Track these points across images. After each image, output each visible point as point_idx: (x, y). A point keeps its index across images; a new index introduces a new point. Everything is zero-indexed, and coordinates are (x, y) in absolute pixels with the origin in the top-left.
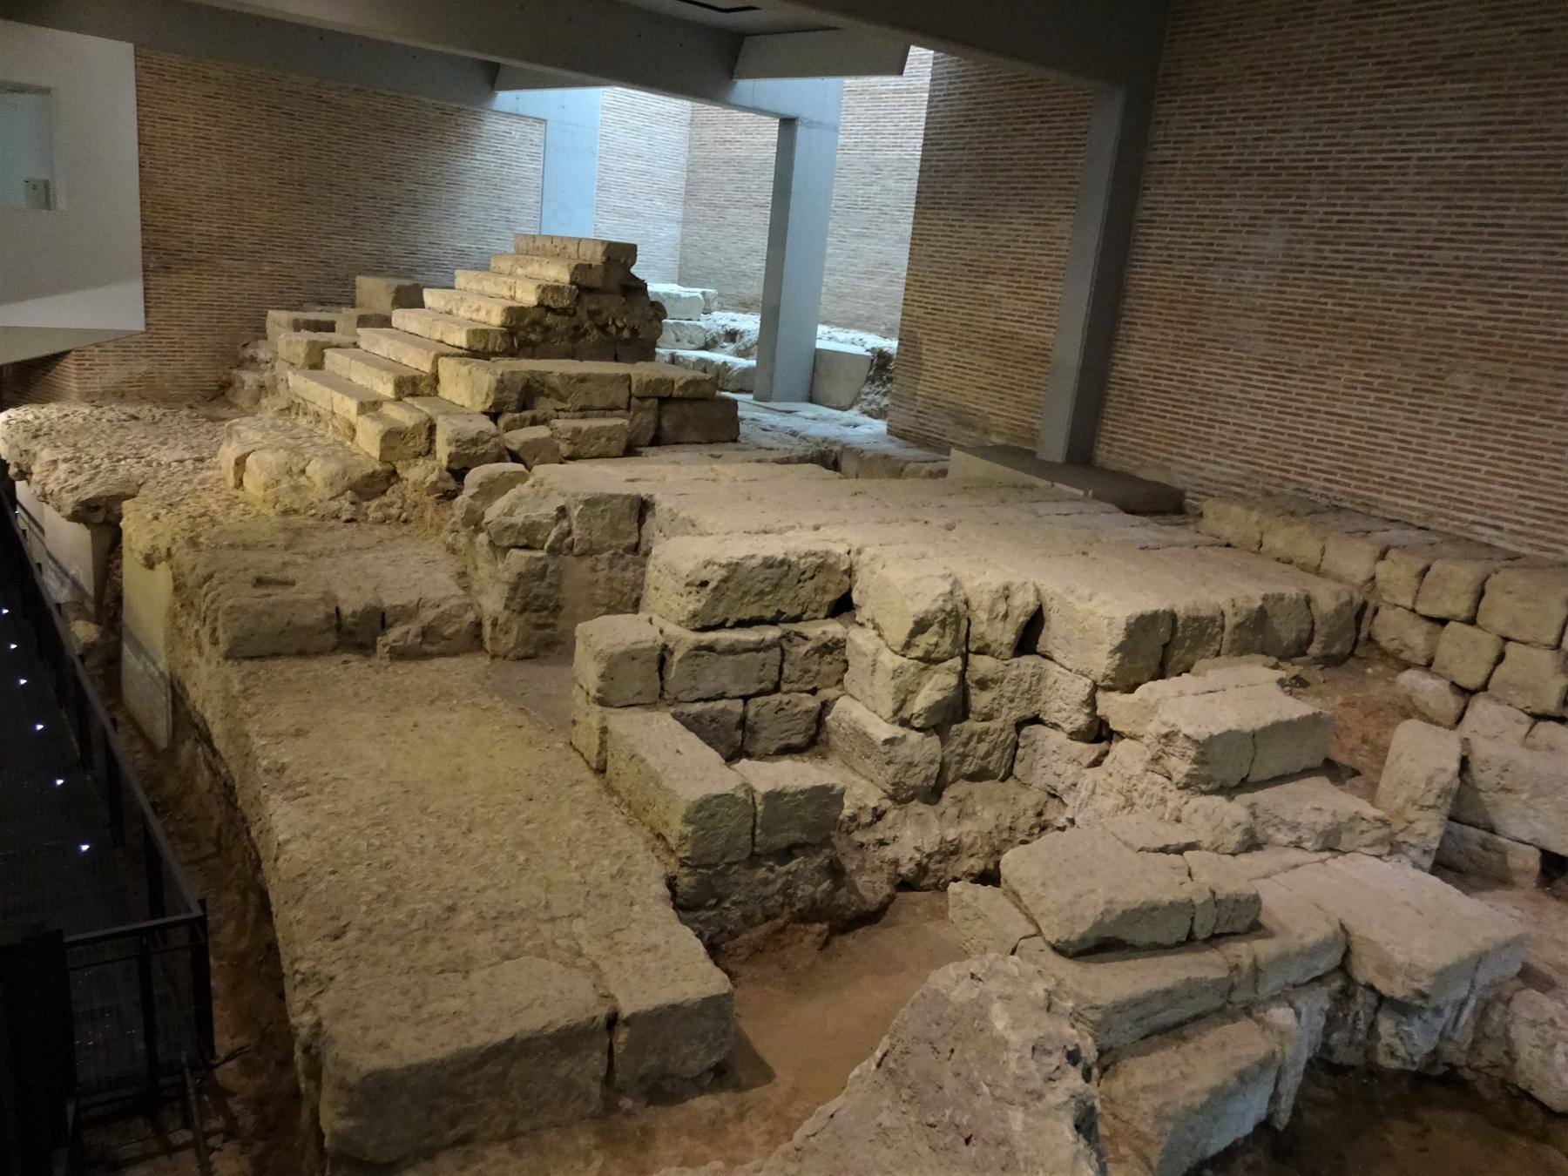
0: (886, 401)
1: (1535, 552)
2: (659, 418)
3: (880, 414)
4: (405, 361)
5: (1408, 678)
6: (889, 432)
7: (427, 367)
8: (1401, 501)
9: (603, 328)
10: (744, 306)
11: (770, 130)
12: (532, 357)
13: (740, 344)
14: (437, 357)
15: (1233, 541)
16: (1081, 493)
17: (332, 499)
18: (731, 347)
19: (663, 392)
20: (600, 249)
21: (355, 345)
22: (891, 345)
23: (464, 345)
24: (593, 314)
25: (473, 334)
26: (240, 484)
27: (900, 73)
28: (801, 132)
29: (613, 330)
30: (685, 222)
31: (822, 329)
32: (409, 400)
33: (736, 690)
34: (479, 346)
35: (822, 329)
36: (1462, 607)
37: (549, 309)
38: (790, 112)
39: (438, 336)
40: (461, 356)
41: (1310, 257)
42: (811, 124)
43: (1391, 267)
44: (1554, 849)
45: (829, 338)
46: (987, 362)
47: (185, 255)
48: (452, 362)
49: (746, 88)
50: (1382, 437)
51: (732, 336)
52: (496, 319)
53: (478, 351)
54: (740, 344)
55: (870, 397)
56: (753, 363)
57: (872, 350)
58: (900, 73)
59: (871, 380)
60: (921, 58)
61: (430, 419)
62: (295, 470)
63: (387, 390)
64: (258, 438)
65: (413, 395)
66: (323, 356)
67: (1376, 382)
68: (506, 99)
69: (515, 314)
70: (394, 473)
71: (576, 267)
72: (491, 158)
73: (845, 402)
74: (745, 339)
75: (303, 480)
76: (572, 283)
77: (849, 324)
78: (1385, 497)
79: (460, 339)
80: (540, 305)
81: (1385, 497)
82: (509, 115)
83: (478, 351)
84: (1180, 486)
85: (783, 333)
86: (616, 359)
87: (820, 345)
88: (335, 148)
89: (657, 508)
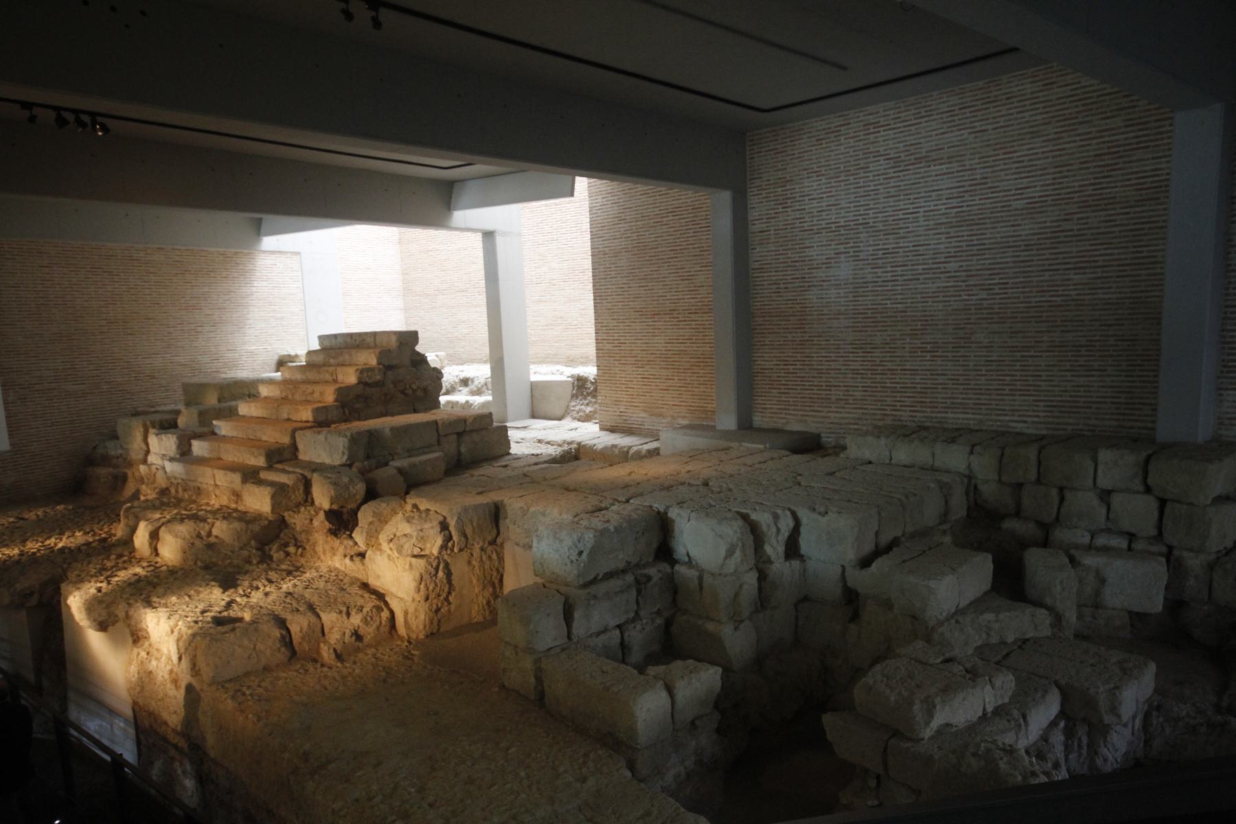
0: (589, 409)
1: (1050, 432)
2: (459, 446)
3: (587, 418)
4: (264, 438)
5: (1007, 524)
6: (602, 429)
7: (286, 440)
8: (960, 416)
9: (403, 392)
10: (585, 363)
11: (477, 240)
12: (359, 419)
13: (472, 387)
14: (294, 431)
15: (872, 459)
16: (762, 447)
17: (241, 549)
18: (465, 390)
19: (460, 430)
20: (394, 338)
21: (214, 433)
22: (590, 371)
23: (311, 419)
24: (395, 383)
25: (317, 411)
26: (156, 552)
27: (572, 195)
28: (499, 240)
29: (410, 392)
30: (406, 309)
31: (533, 368)
32: (279, 466)
33: (613, 623)
34: (321, 418)
35: (533, 368)
36: (1033, 475)
37: (366, 384)
38: (489, 227)
39: (285, 416)
40: (311, 427)
41: (870, 278)
42: (505, 234)
43: (921, 277)
44: (1136, 610)
45: (542, 373)
46: (664, 372)
47: (37, 387)
48: (308, 433)
49: (460, 216)
50: (941, 379)
51: (465, 382)
52: (330, 397)
53: (322, 422)
54: (472, 387)
55: (577, 408)
56: (490, 398)
57: (572, 376)
58: (572, 195)
59: (574, 396)
60: (582, 184)
61: (304, 477)
62: (203, 533)
63: (261, 462)
64: (158, 516)
65: (280, 462)
66: (190, 445)
67: (929, 346)
68: (269, 242)
69: (344, 394)
70: (283, 521)
71: (380, 353)
72: (265, 284)
73: (559, 413)
74: (476, 383)
75: (212, 540)
76: (379, 364)
77: (542, 361)
78: (950, 415)
79: (306, 414)
80: (360, 382)
81: (950, 415)
82: (273, 252)
83: (322, 422)
84: (816, 431)
85: (509, 374)
86: (415, 411)
87: (533, 378)
88: (147, 292)
89: (509, 510)
